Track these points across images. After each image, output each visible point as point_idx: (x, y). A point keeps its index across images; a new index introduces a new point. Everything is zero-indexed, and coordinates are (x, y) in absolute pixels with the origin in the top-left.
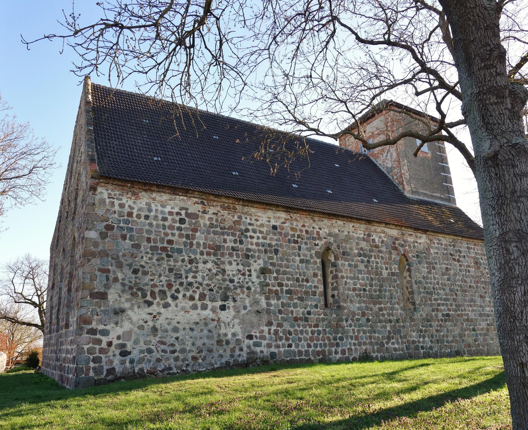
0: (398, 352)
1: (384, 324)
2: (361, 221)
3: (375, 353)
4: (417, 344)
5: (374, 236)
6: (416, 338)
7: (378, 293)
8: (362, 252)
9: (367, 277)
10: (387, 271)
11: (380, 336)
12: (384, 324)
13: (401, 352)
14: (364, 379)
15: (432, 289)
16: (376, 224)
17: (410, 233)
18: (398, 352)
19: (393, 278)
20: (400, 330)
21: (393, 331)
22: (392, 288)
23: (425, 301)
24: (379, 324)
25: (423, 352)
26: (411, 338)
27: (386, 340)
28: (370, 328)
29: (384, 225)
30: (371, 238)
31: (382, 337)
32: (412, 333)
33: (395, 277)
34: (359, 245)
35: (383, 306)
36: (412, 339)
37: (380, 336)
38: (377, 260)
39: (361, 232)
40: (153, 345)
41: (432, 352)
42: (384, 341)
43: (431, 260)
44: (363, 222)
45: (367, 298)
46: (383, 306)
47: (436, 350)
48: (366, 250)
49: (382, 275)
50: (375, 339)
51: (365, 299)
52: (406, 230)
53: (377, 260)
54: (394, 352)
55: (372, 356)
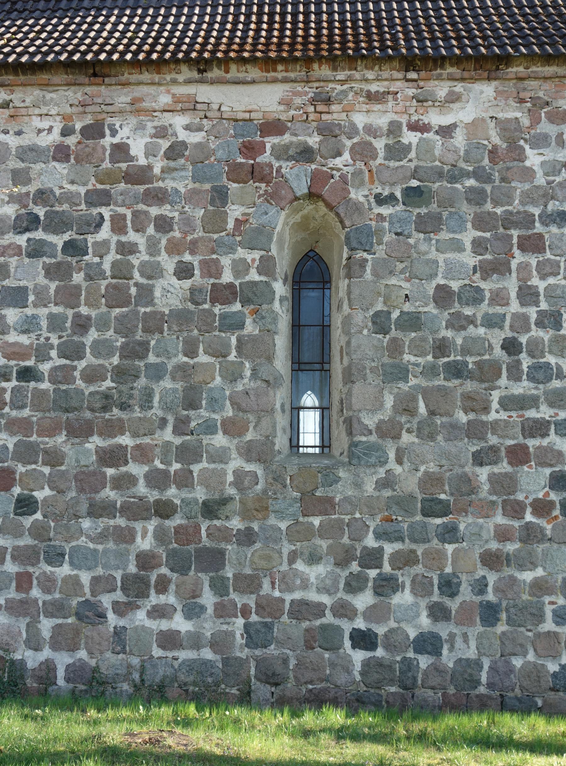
0: (184, 655)
1: (121, 521)
2: (44, 77)
3: (37, 648)
4: (329, 618)
5: (123, 135)
6: (322, 589)
7: (108, 383)
8: (41, 211)
9: (51, 317)
10: (187, 284)
11: (85, 578)
12: (121, 521)
13: (207, 654)
14: (286, 407)
15: (498, 352)
16: (135, 77)
17: (374, 88)
18: (184, 655)
19: (217, 310)
20: (221, 553)
21: (172, 554)
22: (203, 358)
23: (432, 413)
24: (86, 524)
25: (366, 664)
26: (290, 590)
27: (119, 596)
28: (26, 541)
29: (186, 73)
30: (108, 141)
31: (95, 580)
32: (300, 566)
33: (237, 307)
34: (28, 181)
35: (126, 440)
36: (297, 595)
37: (85, 578)
38: (132, 236)
39: (45, 124)
40: (371, 219)
41: (437, 669)
42: (106, 600)
43: (516, 205)
44: (56, 79)
45: (36, 407)
46: (126, 440)
47: (471, 653)
48: (69, 198)
49: (151, 302)
50: (47, 590)
51: (26, 412)
52: (341, 75)
53: (132, 236)
54: (157, 652)
55: (22, 662)
